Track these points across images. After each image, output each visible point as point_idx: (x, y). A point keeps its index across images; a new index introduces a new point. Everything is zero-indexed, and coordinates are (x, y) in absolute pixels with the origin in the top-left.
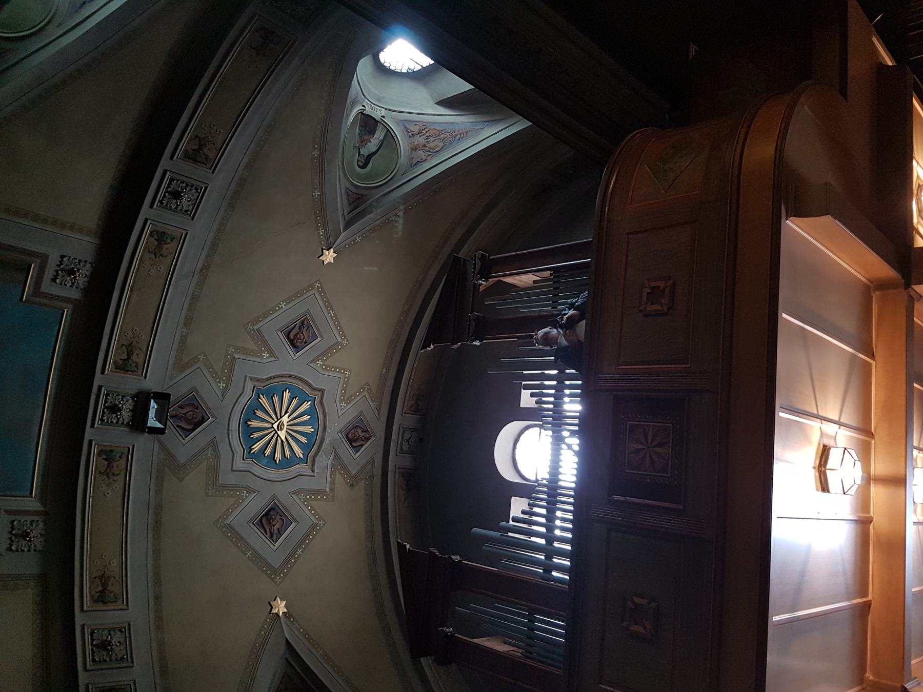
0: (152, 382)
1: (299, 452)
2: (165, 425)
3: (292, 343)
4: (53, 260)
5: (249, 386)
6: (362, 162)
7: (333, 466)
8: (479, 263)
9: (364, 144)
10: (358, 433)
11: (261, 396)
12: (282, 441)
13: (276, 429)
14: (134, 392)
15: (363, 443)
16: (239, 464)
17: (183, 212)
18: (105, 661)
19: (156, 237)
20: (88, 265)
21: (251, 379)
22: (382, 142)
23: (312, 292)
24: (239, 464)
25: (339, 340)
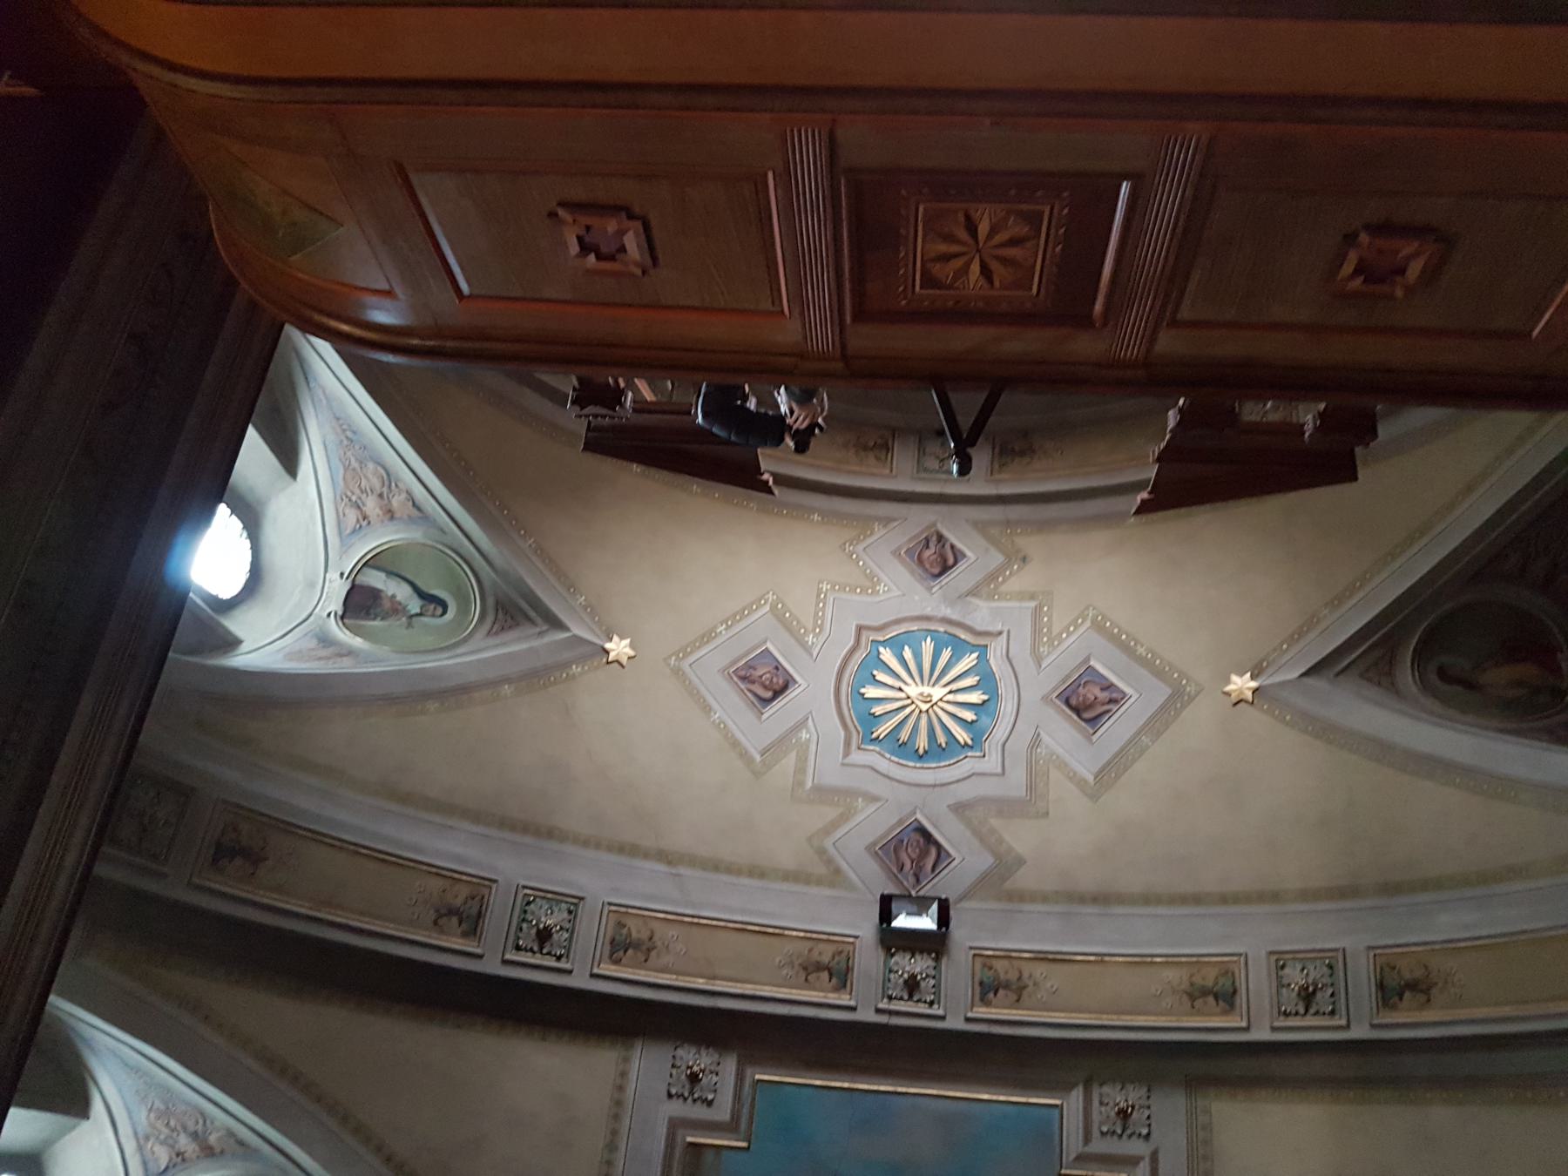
0: (865, 928)
1: (968, 661)
2: (933, 899)
3: (778, 693)
4: (677, 1109)
5: (857, 757)
6: (435, 609)
7: (990, 597)
8: (590, 409)
9: (400, 607)
10: (931, 555)
11: (875, 735)
12: (950, 692)
13: (929, 705)
14: (881, 954)
15: (948, 547)
16: (991, 763)
17: (572, 916)
18: (1332, 995)
19: (621, 953)
20: (680, 1052)
21: (847, 754)
22: (391, 573)
23: (687, 670)
24: (991, 763)
25: (767, 608)
